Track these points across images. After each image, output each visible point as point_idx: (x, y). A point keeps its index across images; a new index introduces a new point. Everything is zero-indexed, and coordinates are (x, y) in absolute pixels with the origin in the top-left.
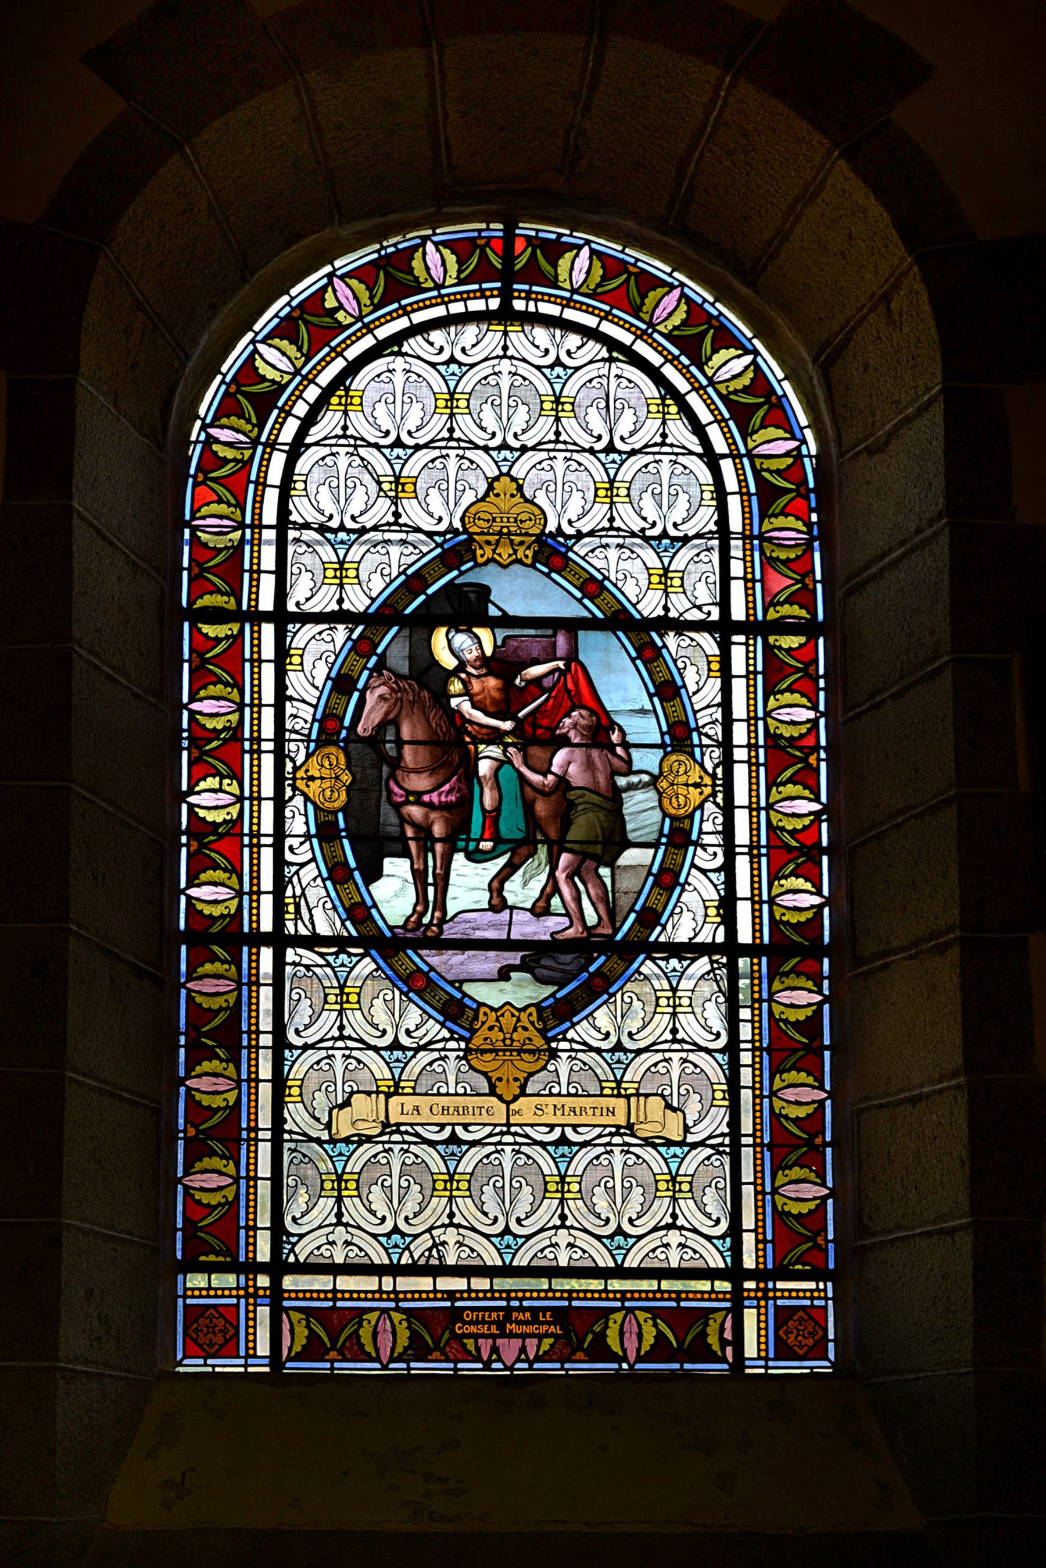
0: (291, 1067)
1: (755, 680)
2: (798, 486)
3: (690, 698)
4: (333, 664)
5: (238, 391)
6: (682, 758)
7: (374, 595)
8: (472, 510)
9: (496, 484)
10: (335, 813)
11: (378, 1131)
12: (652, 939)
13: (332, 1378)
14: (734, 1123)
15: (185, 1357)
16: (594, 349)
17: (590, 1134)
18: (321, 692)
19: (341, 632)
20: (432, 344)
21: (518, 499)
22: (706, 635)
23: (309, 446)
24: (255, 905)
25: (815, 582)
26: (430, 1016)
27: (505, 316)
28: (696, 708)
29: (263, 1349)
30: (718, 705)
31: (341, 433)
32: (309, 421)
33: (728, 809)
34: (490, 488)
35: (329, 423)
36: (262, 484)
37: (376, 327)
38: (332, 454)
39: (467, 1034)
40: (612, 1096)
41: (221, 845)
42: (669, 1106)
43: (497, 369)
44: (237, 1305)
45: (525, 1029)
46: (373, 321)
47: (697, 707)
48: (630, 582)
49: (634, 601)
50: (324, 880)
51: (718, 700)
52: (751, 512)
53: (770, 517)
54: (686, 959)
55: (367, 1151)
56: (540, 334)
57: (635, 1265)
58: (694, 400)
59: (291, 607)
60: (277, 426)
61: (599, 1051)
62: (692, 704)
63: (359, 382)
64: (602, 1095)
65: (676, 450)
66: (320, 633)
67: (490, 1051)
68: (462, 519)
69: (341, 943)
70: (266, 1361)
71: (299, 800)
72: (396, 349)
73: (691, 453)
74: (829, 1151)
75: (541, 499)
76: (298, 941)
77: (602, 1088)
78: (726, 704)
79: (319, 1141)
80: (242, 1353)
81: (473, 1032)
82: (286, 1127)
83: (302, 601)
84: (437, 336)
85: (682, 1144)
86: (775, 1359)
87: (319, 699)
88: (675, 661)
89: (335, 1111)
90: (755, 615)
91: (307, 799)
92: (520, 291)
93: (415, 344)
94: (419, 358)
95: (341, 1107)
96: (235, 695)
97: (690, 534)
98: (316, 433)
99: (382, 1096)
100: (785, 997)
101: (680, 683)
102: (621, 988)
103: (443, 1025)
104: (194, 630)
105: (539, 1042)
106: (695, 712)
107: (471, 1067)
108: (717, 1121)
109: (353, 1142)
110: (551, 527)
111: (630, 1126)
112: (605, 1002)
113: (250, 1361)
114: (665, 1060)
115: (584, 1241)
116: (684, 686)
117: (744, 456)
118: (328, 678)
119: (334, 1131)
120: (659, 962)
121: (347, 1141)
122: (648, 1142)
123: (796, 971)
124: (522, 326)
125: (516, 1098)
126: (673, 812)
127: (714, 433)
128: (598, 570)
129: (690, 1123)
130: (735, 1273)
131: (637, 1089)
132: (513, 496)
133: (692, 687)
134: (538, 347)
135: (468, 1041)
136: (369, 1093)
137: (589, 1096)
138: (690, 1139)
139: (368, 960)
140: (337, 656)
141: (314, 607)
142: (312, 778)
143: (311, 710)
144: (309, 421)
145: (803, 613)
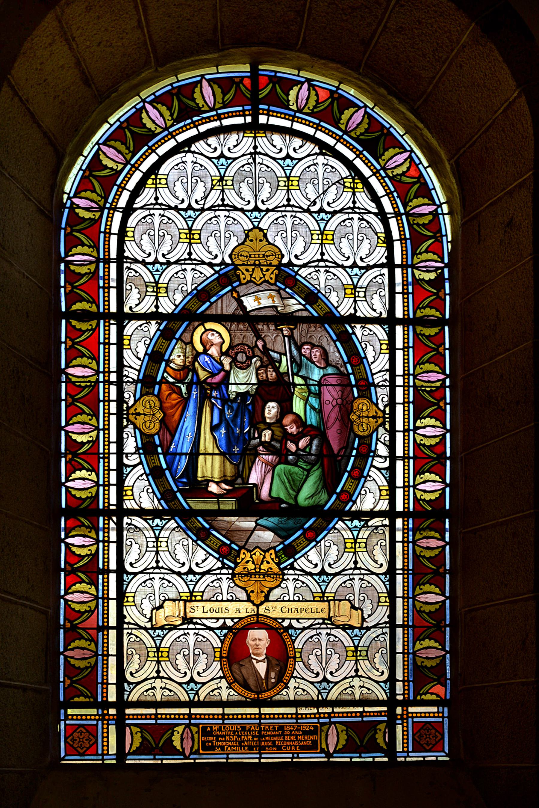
0: (128, 585)
1: (408, 351)
2: (435, 233)
3: (370, 366)
4: (149, 345)
5: (91, 175)
6: (365, 401)
7: (177, 303)
8: (236, 250)
9: (250, 233)
10: (153, 436)
11: (179, 622)
12: (347, 508)
13: (228, 766)
14: (392, 616)
15: (66, 755)
16: (309, 147)
17: (307, 624)
18: (143, 361)
19: (153, 326)
20: (209, 146)
21: (264, 242)
22: (378, 326)
23: (136, 209)
24: (106, 492)
25: (445, 295)
26: (210, 554)
27: (254, 127)
28: (374, 372)
29: (113, 750)
30: (387, 370)
31: (286, 203)
32: (135, 194)
33: (392, 432)
34: (247, 236)
35: (146, 196)
36: (108, 233)
37: (177, 134)
38: (216, 217)
39: (232, 565)
40: (320, 601)
41: (88, 457)
42: (353, 607)
43: (315, 162)
44: (97, 724)
45: (268, 563)
46: (175, 131)
47: (374, 371)
48: (334, 294)
49: (336, 305)
50: (147, 476)
51: (387, 367)
52: (406, 251)
53: (417, 254)
54: (363, 520)
55: (176, 633)
56: (277, 138)
57: (334, 698)
58: (374, 182)
59: (126, 310)
60: (117, 197)
61: (311, 574)
62: (371, 370)
63: (164, 169)
64: (314, 601)
65: (295, 209)
66: (141, 326)
67: (246, 575)
68: (230, 256)
69: (155, 514)
70: (114, 757)
71: (130, 428)
72: (186, 149)
73: (370, 212)
74: (448, 629)
75: (279, 243)
76: (132, 512)
77: (314, 597)
78: (392, 369)
79: (146, 629)
80: (100, 752)
81: (237, 564)
82: (126, 620)
83: (133, 306)
84: (212, 140)
85: (361, 628)
86: (413, 751)
87: (141, 366)
88: (360, 343)
89: (154, 611)
90: (408, 315)
91: (135, 427)
92: (263, 110)
93: (200, 146)
94: (202, 154)
95: (158, 609)
96: (94, 365)
97: (371, 264)
98: (139, 202)
99: (182, 603)
100: (424, 543)
101: (363, 355)
102: (324, 537)
103: (218, 559)
104: (68, 323)
105: (276, 569)
106: (373, 375)
107: (236, 585)
108: (382, 614)
109: (166, 629)
110: (285, 261)
111: (330, 619)
112: (314, 546)
113: (105, 757)
114: (351, 580)
115: (369, 684)
116: (366, 357)
117: (403, 214)
118: (146, 354)
119: (154, 623)
120: (346, 522)
121: (162, 628)
122: (338, 627)
123: (430, 528)
124: (265, 133)
125: (262, 603)
126: (360, 434)
127: (386, 202)
128: (313, 286)
129: (366, 616)
130: (391, 702)
131: (202, 596)
132: (261, 241)
133: (371, 360)
134: (275, 147)
135: (233, 569)
136: (174, 600)
137: (240, 601)
138: (365, 625)
139: (173, 521)
140: (151, 340)
141: (142, 309)
142: (373, 417)
143: (137, 373)
144: (135, 194)
145: (438, 314)
